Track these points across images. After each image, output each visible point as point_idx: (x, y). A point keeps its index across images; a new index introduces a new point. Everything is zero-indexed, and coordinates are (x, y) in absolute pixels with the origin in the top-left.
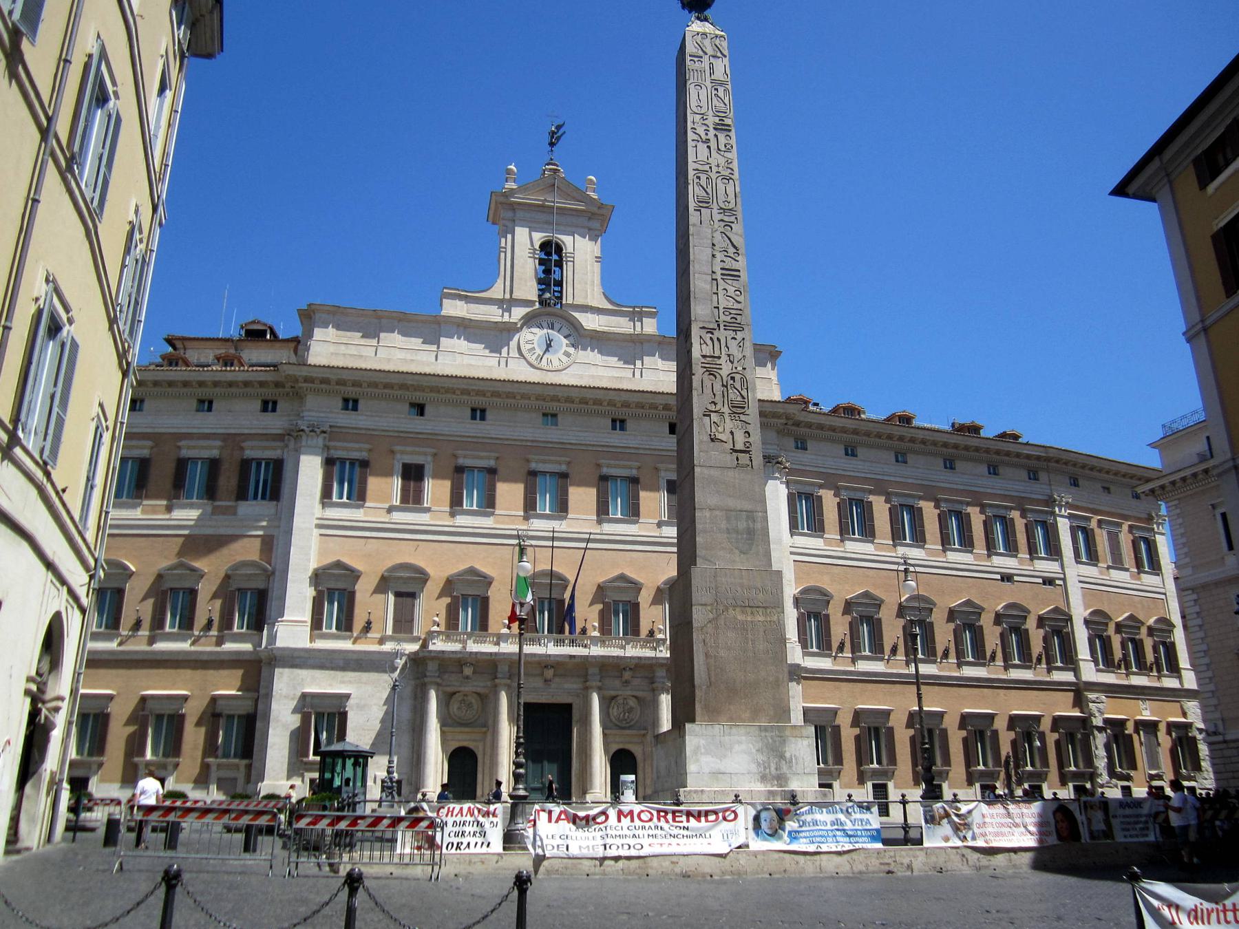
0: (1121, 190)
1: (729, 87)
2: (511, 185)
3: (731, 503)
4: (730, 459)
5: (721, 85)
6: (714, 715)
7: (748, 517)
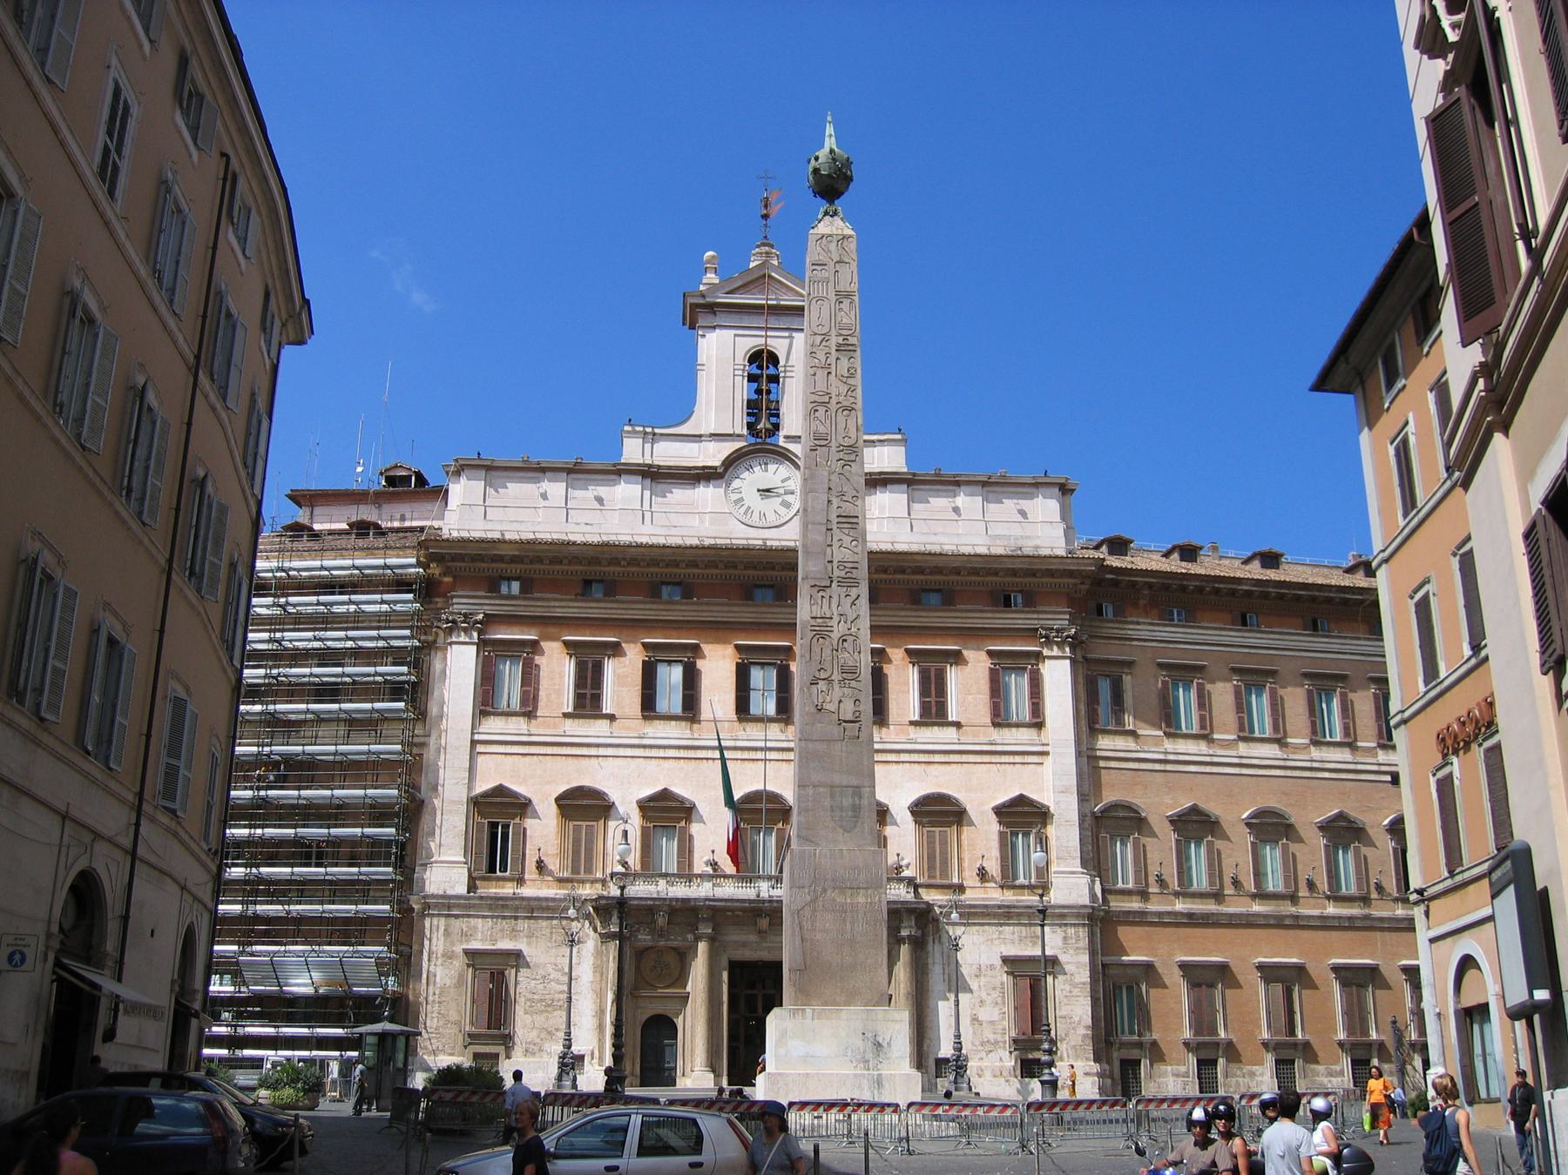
0: (1322, 383)
1: (856, 299)
2: (711, 278)
3: (837, 779)
4: (836, 731)
5: (847, 297)
6: (806, 995)
7: (854, 793)
